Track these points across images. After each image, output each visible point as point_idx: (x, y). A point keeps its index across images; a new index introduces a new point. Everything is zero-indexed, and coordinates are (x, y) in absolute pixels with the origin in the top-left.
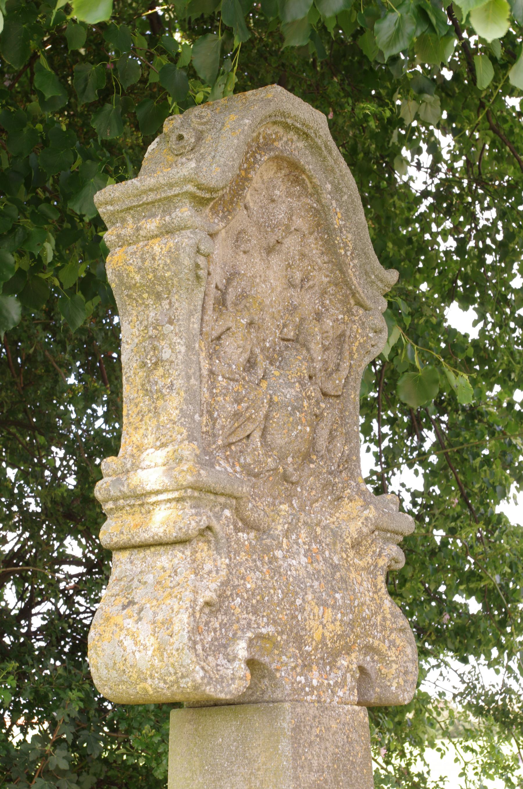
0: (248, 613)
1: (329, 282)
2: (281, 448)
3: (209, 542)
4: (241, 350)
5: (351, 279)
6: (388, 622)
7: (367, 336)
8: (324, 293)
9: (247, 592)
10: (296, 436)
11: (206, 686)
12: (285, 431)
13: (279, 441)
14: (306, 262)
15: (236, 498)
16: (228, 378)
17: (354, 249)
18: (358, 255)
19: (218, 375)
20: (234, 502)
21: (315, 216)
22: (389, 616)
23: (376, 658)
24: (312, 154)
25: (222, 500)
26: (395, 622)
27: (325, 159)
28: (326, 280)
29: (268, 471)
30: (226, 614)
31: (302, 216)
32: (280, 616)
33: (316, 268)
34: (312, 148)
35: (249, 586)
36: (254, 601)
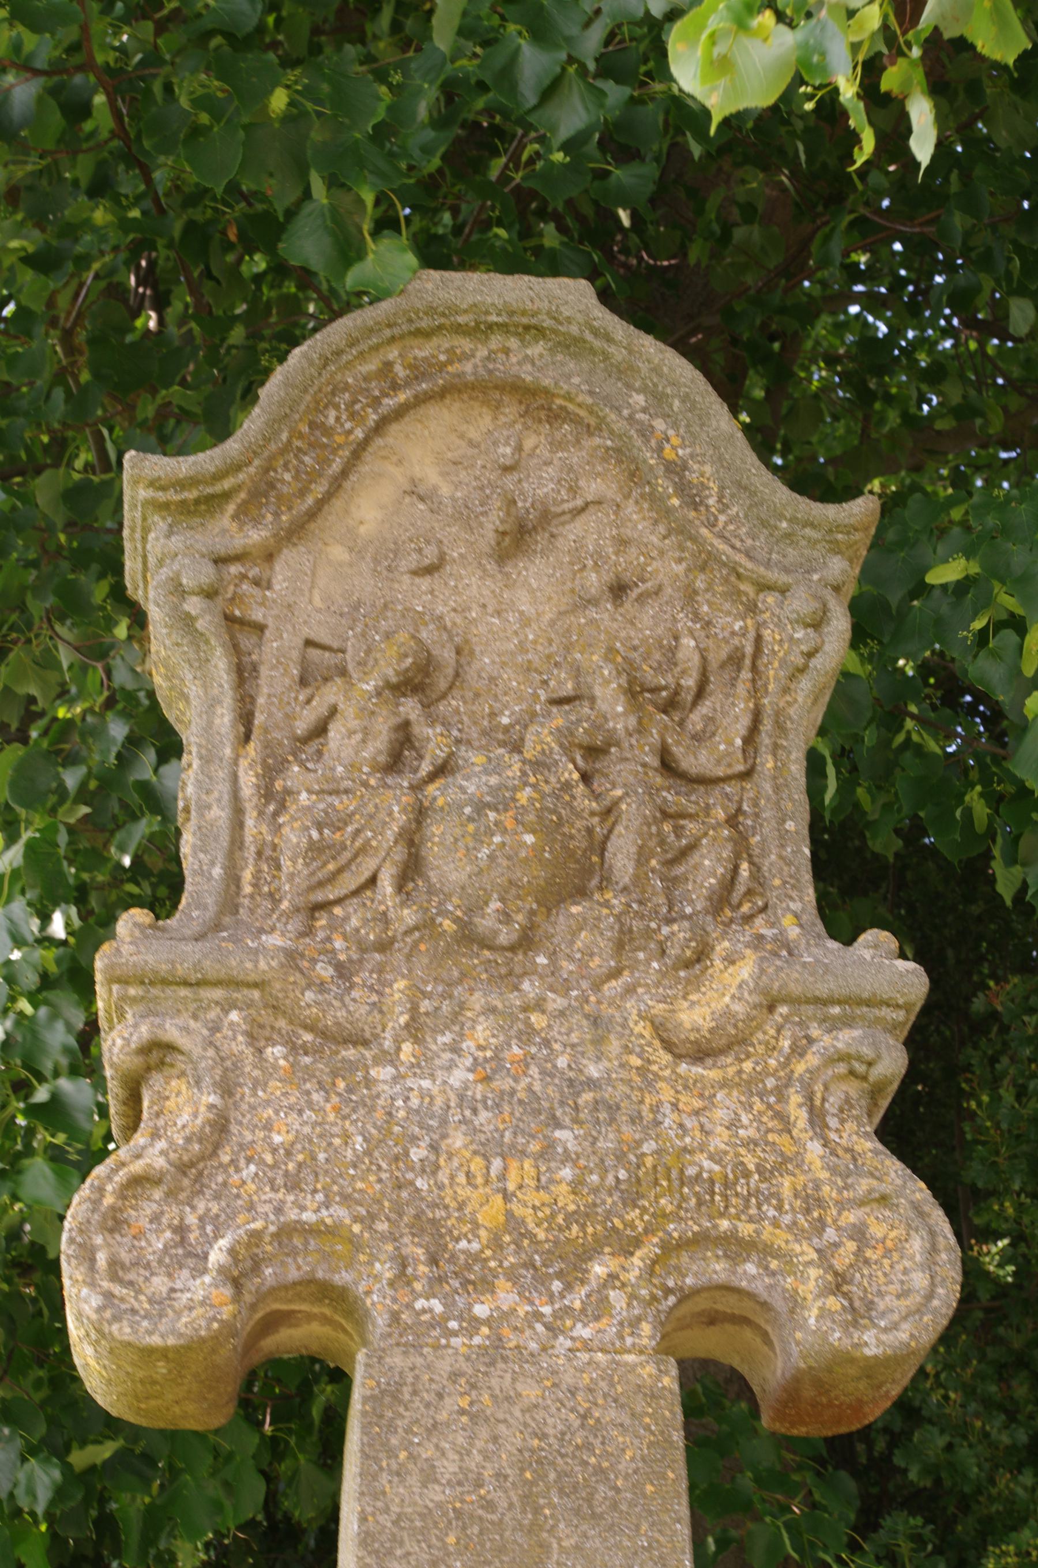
0: (274, 1189)
1: (689, 570)
2: (463, 888)
3: (183, 1074)
4: (359, 736)
5: (712, 545)
6: (826, 1189)
7: (791, 638)
8: (690, 595)
9: (274, 1151)
10: (492, 857)
11: (110, 1324)
12: (459, 855)
13: (454, 877)
14: (633, 551)
15: (256, 985)
16: (322, 792)
17: (722, 488)
18: (733, 496)
19: (299, 793)
20: (256, 994)
21: (620, 462)
22: (824, 1175)
23: (774, 1264)
24: (574, 356)
25: (218, 994)
26: (846, 1187)
27: (606, 357)
28: (679, 569)
29: (408, 932)
30: (217, 1197)
31: (598, 474)
32: (359, 1185)
33: (654, 553)
34: (568, 347)
35: (277, 1139)
36: (291, 1166)
